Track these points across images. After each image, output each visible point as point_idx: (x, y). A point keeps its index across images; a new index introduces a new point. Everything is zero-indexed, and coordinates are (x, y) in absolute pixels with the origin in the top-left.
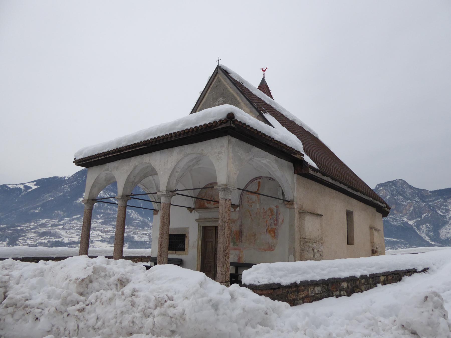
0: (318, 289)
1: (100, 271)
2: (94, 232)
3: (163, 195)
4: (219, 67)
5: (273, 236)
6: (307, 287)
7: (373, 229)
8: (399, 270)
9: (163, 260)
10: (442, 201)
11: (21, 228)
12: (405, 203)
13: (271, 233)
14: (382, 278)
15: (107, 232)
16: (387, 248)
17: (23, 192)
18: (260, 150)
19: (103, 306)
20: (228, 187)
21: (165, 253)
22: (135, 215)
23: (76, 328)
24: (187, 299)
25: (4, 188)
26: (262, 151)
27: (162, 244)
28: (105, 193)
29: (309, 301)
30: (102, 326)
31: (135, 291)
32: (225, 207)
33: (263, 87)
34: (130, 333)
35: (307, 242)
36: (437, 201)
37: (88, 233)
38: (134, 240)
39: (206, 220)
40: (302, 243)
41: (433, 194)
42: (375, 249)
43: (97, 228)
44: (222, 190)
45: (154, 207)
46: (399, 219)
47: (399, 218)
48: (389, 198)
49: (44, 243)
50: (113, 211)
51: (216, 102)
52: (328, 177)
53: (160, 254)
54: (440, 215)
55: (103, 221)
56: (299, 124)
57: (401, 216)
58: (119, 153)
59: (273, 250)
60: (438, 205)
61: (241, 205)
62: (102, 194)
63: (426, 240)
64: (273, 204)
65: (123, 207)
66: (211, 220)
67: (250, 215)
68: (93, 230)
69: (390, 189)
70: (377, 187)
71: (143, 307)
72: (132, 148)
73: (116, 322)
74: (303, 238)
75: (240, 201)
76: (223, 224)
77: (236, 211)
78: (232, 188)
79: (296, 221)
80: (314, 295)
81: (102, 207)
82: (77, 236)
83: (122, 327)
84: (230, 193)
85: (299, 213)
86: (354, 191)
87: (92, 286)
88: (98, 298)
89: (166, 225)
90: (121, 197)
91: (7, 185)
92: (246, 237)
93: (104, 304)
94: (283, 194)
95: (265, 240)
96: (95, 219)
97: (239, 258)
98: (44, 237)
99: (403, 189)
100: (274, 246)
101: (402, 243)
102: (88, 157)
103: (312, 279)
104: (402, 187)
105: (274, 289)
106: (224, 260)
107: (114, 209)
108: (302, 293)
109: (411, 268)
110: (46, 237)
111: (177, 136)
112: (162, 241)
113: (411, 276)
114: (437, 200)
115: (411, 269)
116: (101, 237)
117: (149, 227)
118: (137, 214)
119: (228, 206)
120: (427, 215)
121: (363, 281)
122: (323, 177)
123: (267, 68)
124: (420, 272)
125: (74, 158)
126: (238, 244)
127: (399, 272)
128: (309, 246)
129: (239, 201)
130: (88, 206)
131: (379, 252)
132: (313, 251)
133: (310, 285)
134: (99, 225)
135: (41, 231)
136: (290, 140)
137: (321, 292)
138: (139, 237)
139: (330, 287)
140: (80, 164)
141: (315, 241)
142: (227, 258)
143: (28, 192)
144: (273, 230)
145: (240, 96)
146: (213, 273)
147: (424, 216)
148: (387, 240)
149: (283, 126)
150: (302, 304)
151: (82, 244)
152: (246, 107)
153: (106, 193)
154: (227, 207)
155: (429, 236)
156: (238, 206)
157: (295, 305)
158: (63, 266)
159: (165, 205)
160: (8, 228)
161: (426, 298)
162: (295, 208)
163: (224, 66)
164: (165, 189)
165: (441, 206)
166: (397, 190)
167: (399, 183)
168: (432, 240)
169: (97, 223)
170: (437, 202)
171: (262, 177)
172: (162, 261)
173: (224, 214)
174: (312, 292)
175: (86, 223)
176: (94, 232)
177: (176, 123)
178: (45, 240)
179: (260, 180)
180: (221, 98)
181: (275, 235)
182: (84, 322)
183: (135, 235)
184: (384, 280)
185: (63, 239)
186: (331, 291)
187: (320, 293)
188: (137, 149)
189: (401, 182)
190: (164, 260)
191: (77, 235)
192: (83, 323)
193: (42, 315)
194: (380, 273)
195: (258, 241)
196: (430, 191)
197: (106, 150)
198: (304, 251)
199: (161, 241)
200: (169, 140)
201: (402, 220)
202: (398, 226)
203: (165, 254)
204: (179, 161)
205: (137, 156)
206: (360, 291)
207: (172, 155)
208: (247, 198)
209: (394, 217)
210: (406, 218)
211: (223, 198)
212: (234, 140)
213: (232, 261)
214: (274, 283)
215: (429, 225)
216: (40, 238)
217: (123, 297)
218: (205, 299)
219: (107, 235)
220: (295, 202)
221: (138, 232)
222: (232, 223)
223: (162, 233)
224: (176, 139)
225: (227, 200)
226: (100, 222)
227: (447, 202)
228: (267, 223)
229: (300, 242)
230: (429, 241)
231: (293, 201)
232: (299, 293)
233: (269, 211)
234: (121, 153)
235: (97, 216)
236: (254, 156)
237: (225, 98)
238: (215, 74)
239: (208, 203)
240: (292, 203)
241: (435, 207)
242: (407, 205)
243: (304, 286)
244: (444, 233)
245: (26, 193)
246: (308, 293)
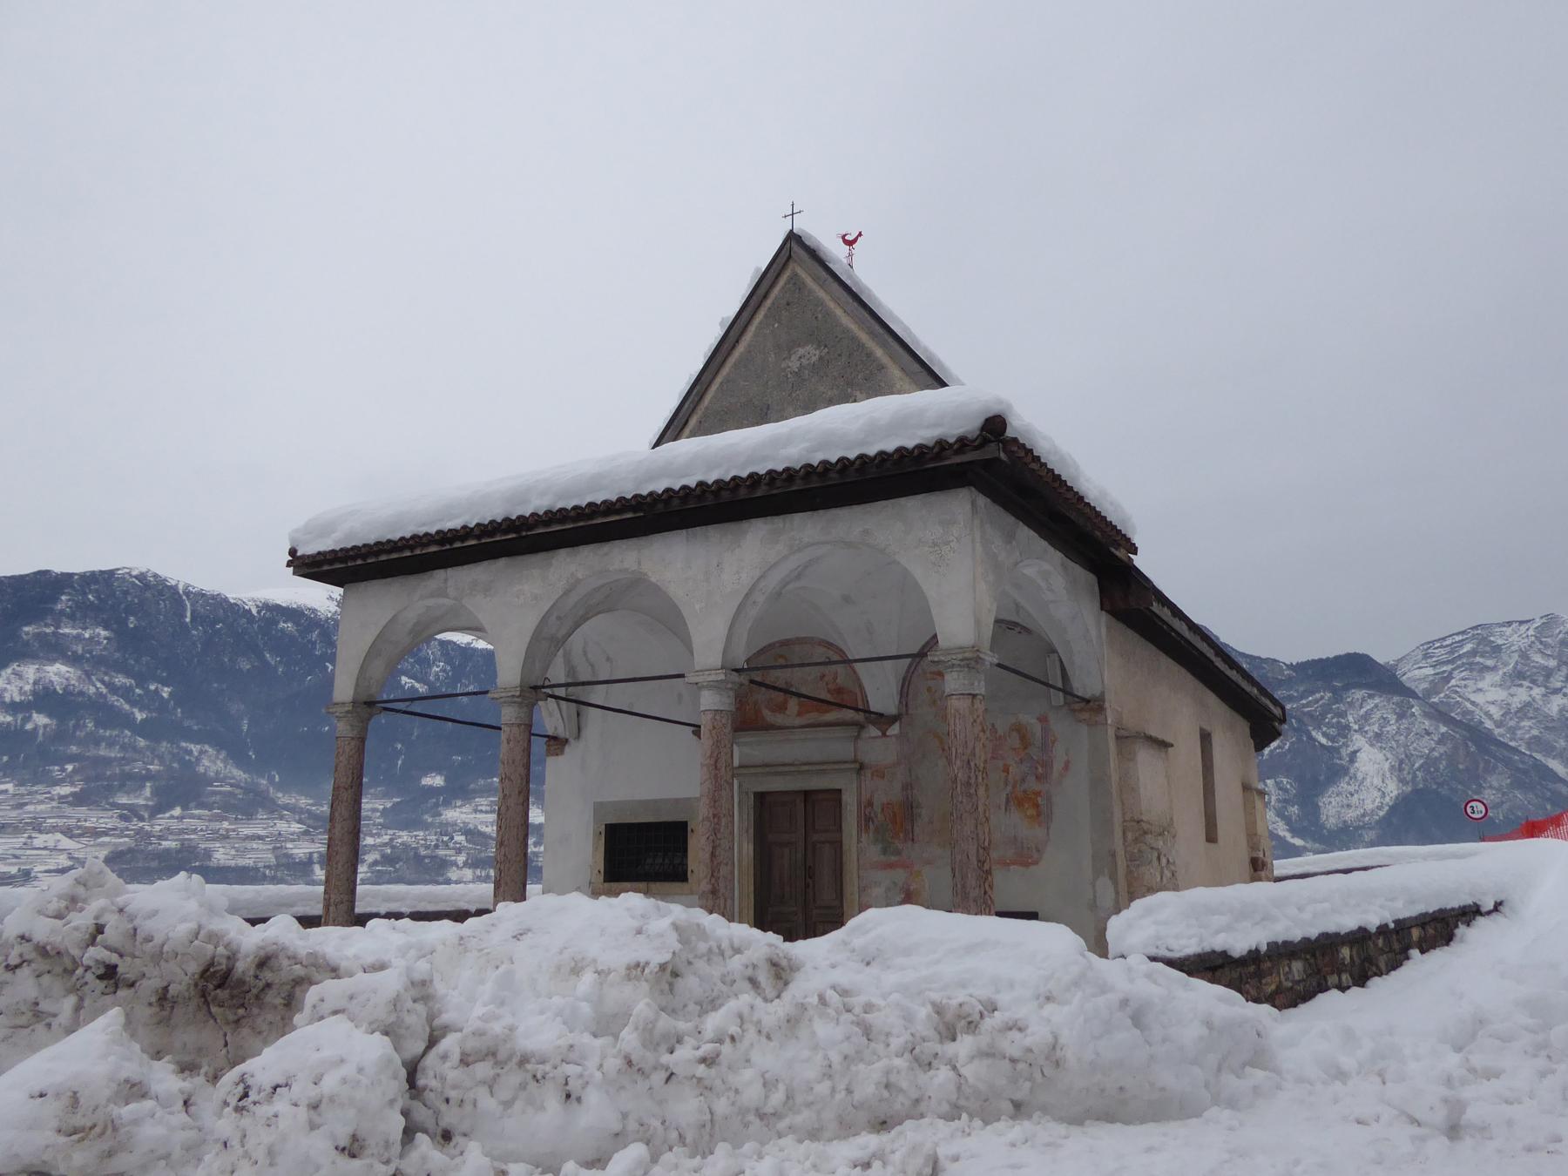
1: (694, 938)
2: (37, 835)
3: (711, 683)
4: (793, 238)
10: (1326, 698)
13: (1027, 806)
15: (95, 833)
19: (772, 1044)
22: (215, 763)
23: (708, 1117)
24: (1053, 1002)
27: (717, 853)
28: (89, 679)
30: (785, 1103)
32: (972, 720)
34: (881, 1121)
36: (1310, 698)
37: (355, 827)
38: (212, 864)
39: (770, 768)
40: (1130, 836)
41: (1297, 674)
43: (48, 821)
44: (959, 665)
45: (548, 727)
50: (123, 748)
53: (713, 885)
54: (1322, 745)
55: (77, 789)
59: (1036, 863)
60: (1315, 711)
61: (907, 714)
62: (73, 682)
63: (1275, 832)
65: (523, 726)
66: (792, 769)
68: (33, 829)
71: (907, 1037)
73: (833, 1090)
74: (1132, 820)
75: (900, 702)
76: (969, 777)
77: (888, 736)
79: (1112, 765)
81: (74, 732)
83: (854, 1103)
85: (1117, 738)
90: (518, 694)
93: (771, 1036)
95: (1003, 830)
96: (38, 784)
107: (126, 740)
111: (778, 483)
114: (1313, 693)
116: (69, 858)
117: (276, 811)
118: (224, 761)
120: (1279, 747)
123: (860, 234)
124: (1489, 913)
126: (900, 846)
129: (897, 703)
130: (352, 726)
134: (58, 807)
136: (1112, 504)
138: (233, 852)
140: (308, 574)
144: (1033, 796)
147: (1271, 751)
151: (337, 869)
153: (94, 678)
155: (1288, 820)
156: (893, 719)
158: (520, 932)
159: (718, 717)
163: (811, 237)
164: (719, 664)
165: (1323, 715)
168: (1295, 832)
169: (52, 799)
170: (1310, 701)
173: (970, 745)
176: (33, 835)
180: (809, 348)
181: (1039, 815)
182: (728, 1098)
183: (218, 845)
188: (599, 522)
192: (723, 1101)
193: (587, 1083)
196: (1288, 663)
198: (1138, 862)
203: (728, 887)
205: (581, 548)
206: (1378, 971)
207: (739, 546)
208: (929, 689)
211: (964, 692)
212: (982, 500)
214: (1214, 952)
215: (1285, 781)
219: (93, 849)
220: (1107, 705)
221: (227, 830)
222: (872, 779)
224: (775, 492)
226: (66, 797)
227: (1341, 701)
228: (1008, 773)
230: (1285, 837)
232: (1264, 981)
233: (1015, 734)
235: (51, 771)
237: (826, 346)
239: (773, 712)
240: (1098, 705)
241: (1305, 719)
244: (1334, 807)
246: (1280, 982)
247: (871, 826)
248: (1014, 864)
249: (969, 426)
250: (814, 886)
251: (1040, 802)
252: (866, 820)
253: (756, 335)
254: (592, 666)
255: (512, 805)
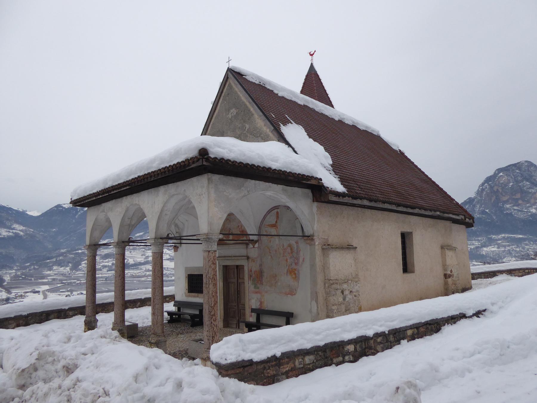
0: (308, 359)
1: (48, 356)
4: (229, 70)
5: (293, 278)
6: (293, 358)
7: (446, 249)
8: (437, 319)
9: (158, 319)
11: (83, 251)
12: (533, 191)
13: (292, 274)
14: (409, 332)
16: (511, 247)
17: (79, 212)
18: (257, 182)
20: (210, 237)
21: (159, 311)
25: (59, 208)
26: (261, 182)
29: (296, 374)
31: (78, 381)
33: (312, 76)
35: (333, 284)
40: (327, 285)
42: (449, 272)
46: (525, 211)
47: (526, 210)
48: (512, 185)
49: (109, 266)
51: (228, 114)
52: (362, 200)
56: (350, 123)
57: (529, 207)
58: (107, 194)
59: (295, 295)
61: (260, 240)
64: (292, 241)
65: (120, 255)
67: (270, 253)
69: (513, 174)
70: (497, 172)
72: (118, 189)
76: (207, 281)
78: (216, 237)
80: (303, 366)
82: (142, 256)
84: (214, 244)
86: (409, 209)
87: (36, 375)
88: (33, 393)
89: (158, 278)
91: (62, 205)
92: (267, 278)
94: (302, 229)
95: (286, 282)
97: (261, 303)
98: (107, 259)
99: (530, 173)
100: (295, 290)
101: (530, 240)
102: (81, 198)
103: (300, 348)
104: (529, 171)
105: (244, 367)
106: (210, 323)
108: (285, 366)
109: (458, 313)
110: (109, 259)
112: (155, 297)
113: (456, 323)
115: (457, 315)
119: (212, 259)
121: (379, 340)
122: (355, 201)
123: (315, 51)
124: (471, 317)
125: (71, 198)
126: (259, 286)
127: (437, 321)
128: (336, 288)
130: (90, 252)
131: (455, 275)
132: (343, 294)
133: (298, 355)
135: (103, 254)
137: (314, 361)
139: (328, 353)
141: (346, 281)
142: (214, 320)
143: (84, 211)
145: (253, 107)
146: (237, 319)
148: (512, 237)
149: (310, 137)
150: (285, 379)
152: (260, 120)
154: (211, 260)
157: (275, 381)
160: (69, 252)
161: (398, 388)
162: (316, 244)
164: (154, 238)
166: (521, 174)
167: (524, 166)
171: (280, 206)
172: (155, 319)
174: (300, 363)
175: (89, 272)
177: (152, 161)
178: (109, 263)
179: (278, 210)
180: (234, 110)
184: (412, 334)
185: (128, 260)
186: (330, 358)
187: (313, 362)
189: (527, 164)
190: (159, 319)
191: (142, 255)
194: (406, 327)
195: (279, 284)
197: (95, 191)
199: (154, 297)
200: (149, 180)
201: (530, 212)
202: (524, 219)
203: (159, 312)
204: (165, 204)
209: (519, 209)
210: (535, 209)
211: (206, 250)
213: (254, 307)
214: (243, 361)
216: (104, 261)
217: (59, 391)
218: (136, 396)
220: (315, 237)
223: (154, 288)
224: (155, 179)
225: (210, 252)
228: (287, 262)
229: (325, 284)
231: (313, 236)
232: (281, 367)
233: (289, 248)
234: (110, 193)
236: (248, 192)
237: (238, 109)
238: (225, 79)
242: (535, 192)
243: (287, 358)
245: (82, 212)
247: (252, 279)
248: (289, 294)
249: (193, 153)
250: (240, 297)
251: (296, 273)
252: (250, 276)
253: (220, 107)
254: (182, 223)
255: (117, 280)
